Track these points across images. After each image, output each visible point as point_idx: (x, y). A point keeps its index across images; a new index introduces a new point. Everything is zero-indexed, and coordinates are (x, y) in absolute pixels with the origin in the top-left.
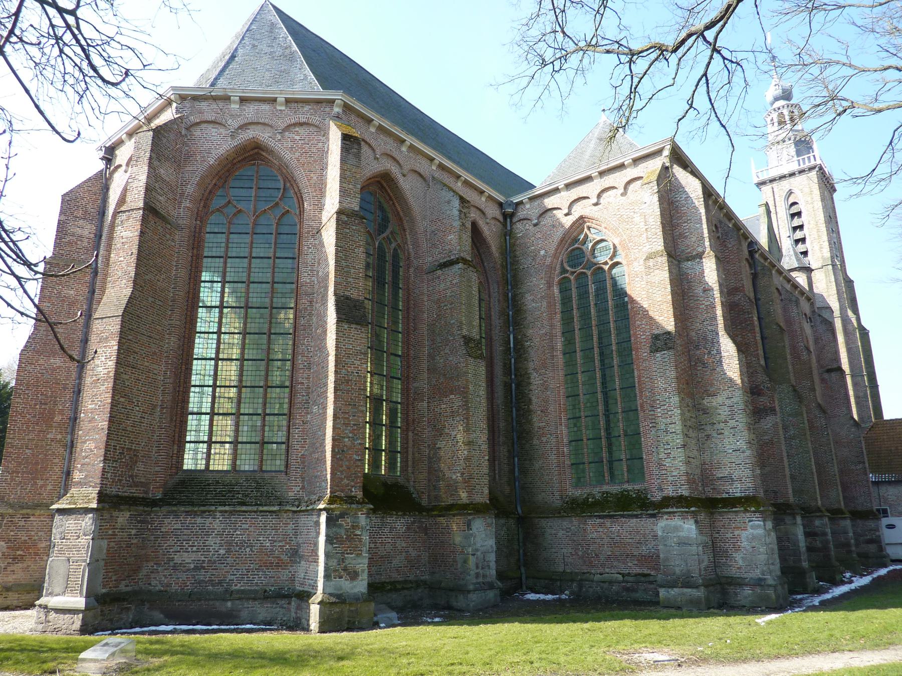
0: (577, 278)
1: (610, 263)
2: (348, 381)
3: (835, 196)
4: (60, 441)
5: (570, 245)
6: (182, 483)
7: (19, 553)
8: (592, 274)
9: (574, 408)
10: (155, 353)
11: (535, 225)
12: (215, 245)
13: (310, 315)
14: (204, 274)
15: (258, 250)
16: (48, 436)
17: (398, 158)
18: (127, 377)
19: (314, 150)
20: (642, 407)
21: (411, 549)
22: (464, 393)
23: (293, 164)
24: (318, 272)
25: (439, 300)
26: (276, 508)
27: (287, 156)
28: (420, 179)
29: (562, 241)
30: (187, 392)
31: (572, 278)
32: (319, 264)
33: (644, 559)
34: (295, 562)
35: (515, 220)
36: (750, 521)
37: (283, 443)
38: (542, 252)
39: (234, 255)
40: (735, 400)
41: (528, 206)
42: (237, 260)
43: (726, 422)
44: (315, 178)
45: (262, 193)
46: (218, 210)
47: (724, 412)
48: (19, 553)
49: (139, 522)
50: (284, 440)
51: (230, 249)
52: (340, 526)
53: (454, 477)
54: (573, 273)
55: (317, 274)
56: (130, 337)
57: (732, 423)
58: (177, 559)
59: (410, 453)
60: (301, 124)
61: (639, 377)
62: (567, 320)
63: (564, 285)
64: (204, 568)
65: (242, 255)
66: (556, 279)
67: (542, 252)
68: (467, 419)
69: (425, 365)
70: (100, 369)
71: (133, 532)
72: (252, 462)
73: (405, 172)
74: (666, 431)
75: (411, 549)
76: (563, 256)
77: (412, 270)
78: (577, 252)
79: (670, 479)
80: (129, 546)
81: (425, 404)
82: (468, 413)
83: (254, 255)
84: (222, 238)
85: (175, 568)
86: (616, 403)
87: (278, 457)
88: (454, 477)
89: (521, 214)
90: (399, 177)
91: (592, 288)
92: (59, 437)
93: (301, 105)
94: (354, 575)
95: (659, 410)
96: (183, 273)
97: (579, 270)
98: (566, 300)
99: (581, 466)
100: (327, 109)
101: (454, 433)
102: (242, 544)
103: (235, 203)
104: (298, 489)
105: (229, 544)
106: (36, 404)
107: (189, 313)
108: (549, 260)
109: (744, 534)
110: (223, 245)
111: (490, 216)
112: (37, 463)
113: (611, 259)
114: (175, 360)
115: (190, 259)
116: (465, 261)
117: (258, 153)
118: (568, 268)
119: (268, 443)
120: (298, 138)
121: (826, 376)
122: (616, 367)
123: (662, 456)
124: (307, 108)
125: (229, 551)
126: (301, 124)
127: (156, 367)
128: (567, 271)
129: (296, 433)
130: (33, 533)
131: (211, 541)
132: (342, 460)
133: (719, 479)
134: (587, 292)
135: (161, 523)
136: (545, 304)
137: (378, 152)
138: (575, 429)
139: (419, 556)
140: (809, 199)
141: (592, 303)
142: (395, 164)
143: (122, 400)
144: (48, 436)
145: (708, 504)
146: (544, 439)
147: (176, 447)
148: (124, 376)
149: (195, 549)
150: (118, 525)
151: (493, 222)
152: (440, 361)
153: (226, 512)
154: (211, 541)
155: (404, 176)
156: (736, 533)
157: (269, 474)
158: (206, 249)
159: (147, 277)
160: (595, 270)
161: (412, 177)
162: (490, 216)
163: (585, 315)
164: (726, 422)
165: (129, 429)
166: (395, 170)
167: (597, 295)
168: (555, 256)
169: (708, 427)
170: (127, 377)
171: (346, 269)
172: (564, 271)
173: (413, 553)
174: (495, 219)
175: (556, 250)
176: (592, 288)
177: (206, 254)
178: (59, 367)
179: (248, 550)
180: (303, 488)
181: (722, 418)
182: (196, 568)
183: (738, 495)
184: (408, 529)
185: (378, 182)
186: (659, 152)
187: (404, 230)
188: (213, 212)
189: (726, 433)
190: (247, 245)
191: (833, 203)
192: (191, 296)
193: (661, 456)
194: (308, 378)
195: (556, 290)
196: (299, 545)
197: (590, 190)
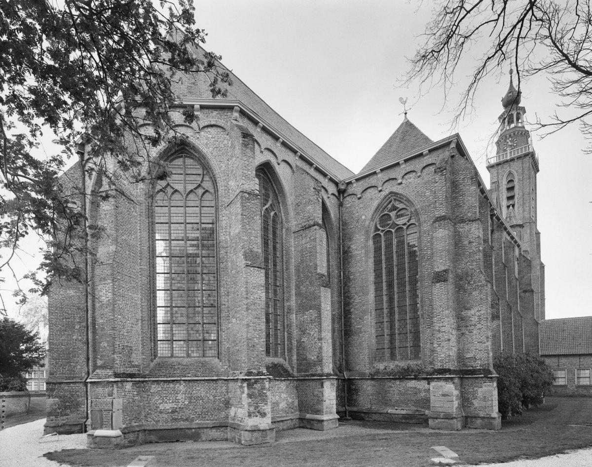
0: (385, 235)
1: (408, 224)
2: (254, 304)
3: (538, 175)
4: (81, 340)
5: (382, 212)
6: (160, 366)
7: (67, 404)
8: (396, 232)
9: (380, 317)
10: (134, 287)
11: (359, 198)
12: (162, 215)
13: (227, 261)
14: (157, 235)
15: (190, 218)
16: (74, 338)
17: (275, 152)
18: (120, 303)
19: (222, 145)
20: (422, 315)
21: (289, 398)
22: (319, 309)
23: (209, 156)
24: (230, 233)
25: (302, 250)
26: (215, 378)
27: (205, 150)
28: (288, 166)
29: (376, 209)
30: (155, 311)
31: (382, 234)
32: (230, 227)
33: (417, 403)
34: (228, 407)
35: (345, 195)
36: (484, 383)
37: (215, 340)
38: (363, 217)
39: (175, 221)
40: (482, 312)
41: (355, 185)
42: (178, 225)
43: (475, 325)
44: (224, 166)
45: (189, 178)
46: (161, 190)
47: (474, 319)
48: (67, 404)
49: (137, 387)
50: (215, 338)
51: (172, 218)
52: (255, 388)
53: (313, 358)
54: (383, 231)
55: (230, 235)
56: (119, 277)
57: (479, 326)
58: (161, 407)
59: (286, 344)
60: (212, 126)
61: (422, 298)
62: (378, 262)
63: (377, 237)
64: (177, 412)
65: (179, 221)
66: (372, 235)
67: (363, 217)
68: (320, 324)
69: (293, 292)
70: (104, 298)
71: (135, 393)
72: (167, 349)
73: (279, 162)
74: (439, 331)
75: (289, 398)
76: (377, 220)
77: (284, 230)
78: (386, 217)
79: (440, 359)
80: (134, 401)
81: (294, 316)
82: (320, 322)
83: (187, 221)
84: (166, 210)
85: (161, 412)
86: (406, 314)
87: (213, 348)
88: (313, 358)
89: (350, 190)
90: (275, 165)
91: (395, 241)
92: (80, 338)
93: (211, 110)
94: (263, 415)
95: (436, 318)
96: (145, 235)
97: (387, 229)
98: (377, 250)
99: (383, 350)
100: (229, 114)
101: (312, 333)
102: (197, 398)
103: (172, 185)
104: (226, 367)
105: (190, 398)
106: (63, 319)
107: (151, 261)
108: (367, 223)
109: (480, 390)
110: (167, 215)
111: (330, 193)
112: (69, 354)
113: (408, 221)
114: (147, 291)
115: (147, 225)
116: (318, 225)
117: (183, 148)
118: (380, 228)
119: (207, 340)
120: (210, 136)
121: (522, 294)
122: (407, 292)
123: (435, 345)
124: (215, 113)
125: (190, 402)
126: (212, 126)
127: (135, 295)
128: (379, 230)
129: (224, 335)
130: (74, 393)
131: (179, 397)
132: (253, 351)
133: (467, 358)
134: (391, 244)
135: (150, 388)
136: (363, 251)
137: (263, 147)
138: (380, 329)
139: (293, 402)
140: (521, 177)
141: (395, 251)
142: (272, 156)
143: (119, 317)
144: (74, 338)
145: (465, 374)
146: (361, 335)
147: (153, 344)
148: (118, 302)
149: (171, 401)
150: (127, 390)
151: (332, 197)
152: (303, 289)
153: (186, 380)
154: (179, 397)
155: (279, 164)
156: (475, 389)
157: (209, 358)
158: (156, 218)
159: (123, 237)
160: (397, 229)
161: (283, 165)
162: (330, 193)
163: (389, 259)
164: (475, 325)
165: (125, 334)
166: (273, 161)
167: (397, 246)
168: (372, 219)
169: (463, 329)
170: (120, 303)
171: (249, 231)
172: (377, 229)
173: (290, 400)
174: (333, 194)
175: (373, 215)
176: (395, 241)
177: (157, 221)
178: (73, 296)
179: (201, 401)
180: (230, 366)
181: (473, 323)
182: (173, 412)
183: (479, 368)
184: (287, 387)
185: (261, 169)
186: (449, 144)
187: (279, 203)
188: (158, 192)
189: (475, 332)
190: (183, 215)
191: (536, 180)
192: (151, 250)
193: (434, 346)
194: (228, 301)
195: (371, 243)
196: (230, 399)
197: (397, 173)
